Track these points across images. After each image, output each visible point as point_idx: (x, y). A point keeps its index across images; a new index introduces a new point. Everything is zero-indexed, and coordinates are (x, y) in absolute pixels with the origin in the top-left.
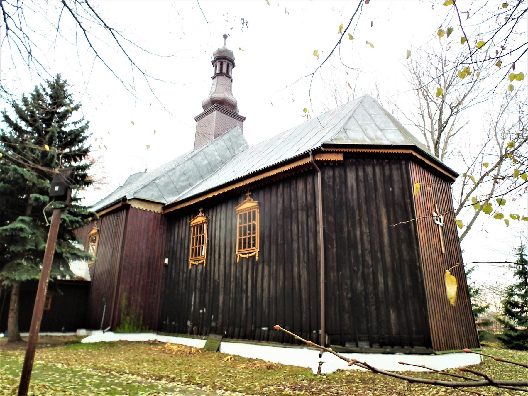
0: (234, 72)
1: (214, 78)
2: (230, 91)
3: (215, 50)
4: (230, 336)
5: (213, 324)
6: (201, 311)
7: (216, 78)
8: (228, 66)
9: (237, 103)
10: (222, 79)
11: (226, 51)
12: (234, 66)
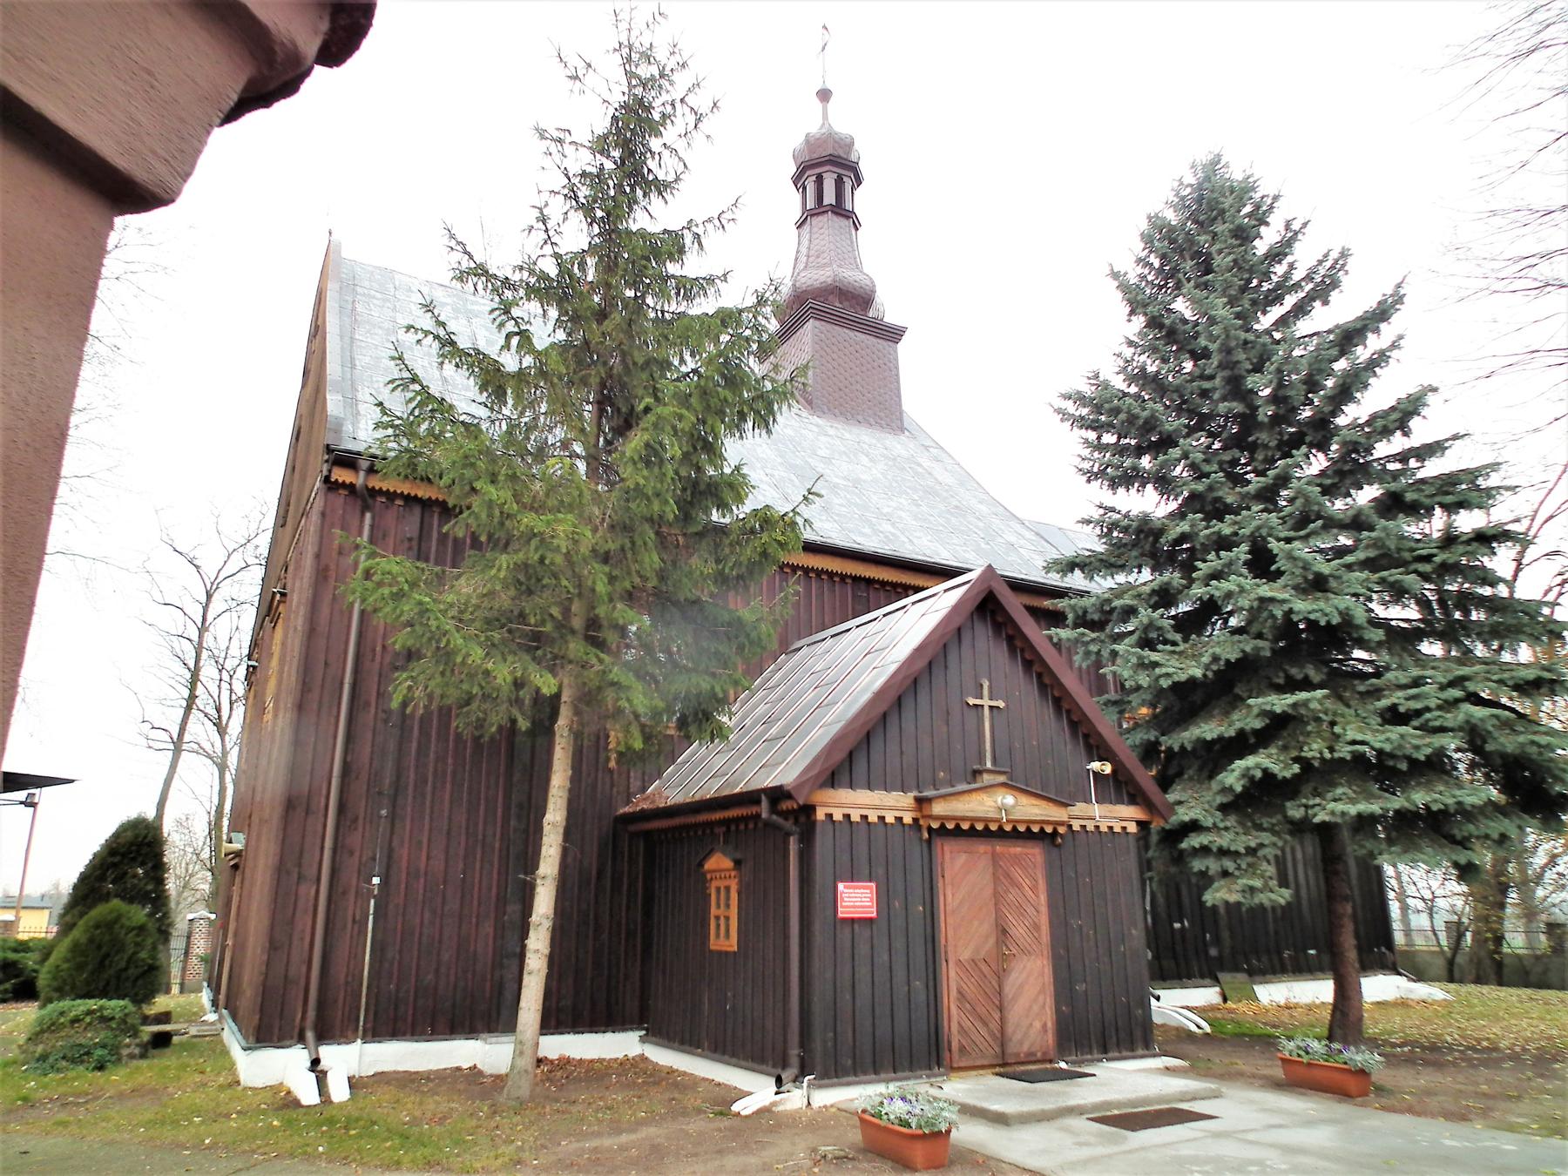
0: (861, 200)
1: (800, 226)
2: (858, 267)
3: (797, 141)
5: (1213, 952)
6: (1177, 925)
8: (839, 183)
9: (874, 292)
10: (828, 221)
11: (830, 137)
12: (854, 169)
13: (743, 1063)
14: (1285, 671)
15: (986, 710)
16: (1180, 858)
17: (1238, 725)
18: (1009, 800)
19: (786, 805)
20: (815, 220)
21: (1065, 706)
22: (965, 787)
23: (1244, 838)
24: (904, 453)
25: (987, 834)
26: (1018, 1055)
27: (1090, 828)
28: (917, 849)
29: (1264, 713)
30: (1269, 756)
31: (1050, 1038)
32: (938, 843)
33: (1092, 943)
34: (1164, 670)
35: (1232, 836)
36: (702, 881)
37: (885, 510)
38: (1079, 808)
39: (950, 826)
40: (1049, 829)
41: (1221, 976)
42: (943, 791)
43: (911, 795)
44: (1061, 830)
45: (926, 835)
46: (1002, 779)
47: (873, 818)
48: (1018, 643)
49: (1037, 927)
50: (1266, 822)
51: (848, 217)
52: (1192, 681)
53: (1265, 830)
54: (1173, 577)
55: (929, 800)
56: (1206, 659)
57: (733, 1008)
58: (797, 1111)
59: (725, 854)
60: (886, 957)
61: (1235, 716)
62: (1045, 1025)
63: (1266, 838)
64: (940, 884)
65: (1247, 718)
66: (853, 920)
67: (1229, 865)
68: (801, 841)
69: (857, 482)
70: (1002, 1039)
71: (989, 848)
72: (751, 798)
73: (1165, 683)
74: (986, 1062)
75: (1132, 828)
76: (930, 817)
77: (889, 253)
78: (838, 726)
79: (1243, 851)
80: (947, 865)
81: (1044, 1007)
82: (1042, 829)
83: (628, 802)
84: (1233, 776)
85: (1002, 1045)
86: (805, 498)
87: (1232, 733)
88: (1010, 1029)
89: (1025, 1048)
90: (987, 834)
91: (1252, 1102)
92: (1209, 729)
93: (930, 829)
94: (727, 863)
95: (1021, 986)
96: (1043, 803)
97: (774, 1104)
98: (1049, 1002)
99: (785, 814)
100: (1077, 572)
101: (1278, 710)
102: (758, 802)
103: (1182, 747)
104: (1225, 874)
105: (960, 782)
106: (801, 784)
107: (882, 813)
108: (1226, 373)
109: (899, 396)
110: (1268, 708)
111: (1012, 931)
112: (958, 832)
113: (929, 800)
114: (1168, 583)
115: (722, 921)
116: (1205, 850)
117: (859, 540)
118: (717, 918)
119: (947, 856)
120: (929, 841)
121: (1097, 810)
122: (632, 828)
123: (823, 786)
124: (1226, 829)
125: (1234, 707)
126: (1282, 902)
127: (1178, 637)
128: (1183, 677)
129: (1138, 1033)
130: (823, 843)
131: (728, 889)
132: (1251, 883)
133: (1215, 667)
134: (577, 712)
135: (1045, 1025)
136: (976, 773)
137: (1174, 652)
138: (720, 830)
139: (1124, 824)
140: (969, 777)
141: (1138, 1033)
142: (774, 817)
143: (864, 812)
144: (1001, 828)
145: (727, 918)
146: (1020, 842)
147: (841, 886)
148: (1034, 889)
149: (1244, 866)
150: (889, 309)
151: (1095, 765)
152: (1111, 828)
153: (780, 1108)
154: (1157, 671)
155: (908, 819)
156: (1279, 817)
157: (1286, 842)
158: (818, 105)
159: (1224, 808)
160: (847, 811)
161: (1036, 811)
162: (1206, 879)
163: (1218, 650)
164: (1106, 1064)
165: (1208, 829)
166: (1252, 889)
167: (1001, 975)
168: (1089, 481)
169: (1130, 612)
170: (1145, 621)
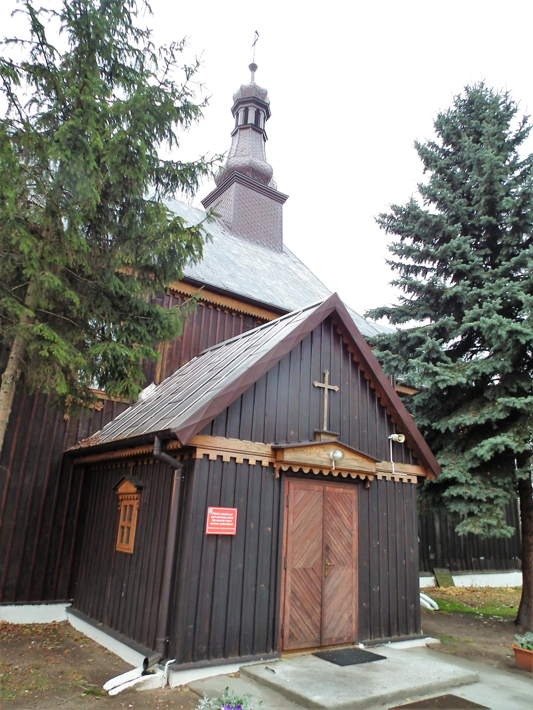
0: (269, 126)
1: (234, 134)
2: (264, 160)
3: (236, 90)
4: (455, 570)
5: (432, 557)
7: (237, 135)
8: (257, 114)
10: (249, 133)
11: (254, 88)
12: (266, 107)
13: (127, 639)
14: (517, 384)
15: (326, 391)
16: (440, 503)
17: (487, 416)
18: (339, 454)
19: (173, 445)
20: (243, 132)
21: (377, 395)
22: (307, 443)
23: (485, 491)
24: (281, 262)
25: (321, 477)
26: (330, 639)
27: (389, 478)
28: (271, 485)
29: (506, 408)
30: (509, 437)
31: (354, 626)
32: (285, 481)
33: (385, 558)
34: (442, 377)
35: (477, 490)
36: (116, 499)
37: (269, 284)
38: (382, 465)
39: (296, 470)
40: (363, 477)
41: (437, 571)
42: (292, 445)
43: (270, 445)
44: (371, 478)
45: (278, 475)
46: (334, 439)
47: (240, 460)
48: (350, 349)
49: (350, 545)
50: (500, 482)
51: (260, 133)
52: (459, 386)
53: (500, 487)
54: (449, 320)
55: (282, 450)
56: (469, 372)
57: (126, 595)
58: (156, 691)
59: (131, 482)
60: (240, 565)
61: (485, 411)
62: (351, 617)
63: (500, 492)
64: (285, 512)
65: (493, 413)
66: (217, 535)
67: (475, 509)
68: (183, 474)
69: (252, 269)
70: (321, 629)
71: (321, 487)
72: (146, 440)
73: (442, 386)
74: (308, 646)
75: (414, 480)
76: (282, 462)
77: (281, 153)
78: (219, 390)
79: (485, 500)
80: (291, 498)
81: (351, 603)
82: (358, 477)
83: (75, 444)
84: (484, 449)
85: (321, 633)
86: (208, 217)
87: (482, 421)
88: (327, 620)
89: (336, 634)
90: (321, 477)
91: (501, 688)
92: (468, 418)
93: (281, 471)
94: (133, 489)
95: (337, 588)
96: (360, 459)
97: (138, 685)
98: (355, 599)
99: (173, 453)
100: (385, 317)
101: (518, 407)
102: (152, 443)
103: (447, 430)
104: (471, 514)
105: (305, 440)
106: (184, 430)
107: (247, 457)
108: (488, 197)
109: (281, 225)
110: (511, 405)
111: (333, 548)
112: (301, 475)
113: (282, 450)
114: (445, 324)
115: (126, 530)
116: (459, 498)
117: (250, 294)
118: (123, 527)
119: (292, 491)
120: (280, 479)
121: (393, 466)
122: (77, 461)
123: (202, 433)
124: (474, 485)
125: (483, 406)
126: (509, 535)
127: (449, 359)
128: (454, 383)
129: (411, 621)
130: (199, 476)
131: (131, 507)
132: (490, 521)
133: (474, 378)
134: (20, 365)
135: (351, 617)
136: (317, 434)
137: (447, 367)
138: (131, 465)
139: (410, 477)
140: (311, 437)
141: (411, 621)
142: (163, 454)
143: (234, 455)
144: (330, 474)
145: (129, 528)
146: (343, 485)
147: (210, 510)
148: (350, 518)
149: (484, 510)
150: (280, 183)
151: (394, 436)
152: (401, 479)
153: (143, 688)
154: (437, 378)
155: (265, 463)
156: (510, 479)
157: (512, 495)
158: (249, 72)
159: (472, 471)
160: (220, 453)
161: (355, 464)
162: (457, 517)
163: (477, 367)
164: (391, 645)
165: (462, 484)
166: (490, 526)
167: (323, 580)
168: (392, 269)
169: (421, 341)
170: (430, 346)
